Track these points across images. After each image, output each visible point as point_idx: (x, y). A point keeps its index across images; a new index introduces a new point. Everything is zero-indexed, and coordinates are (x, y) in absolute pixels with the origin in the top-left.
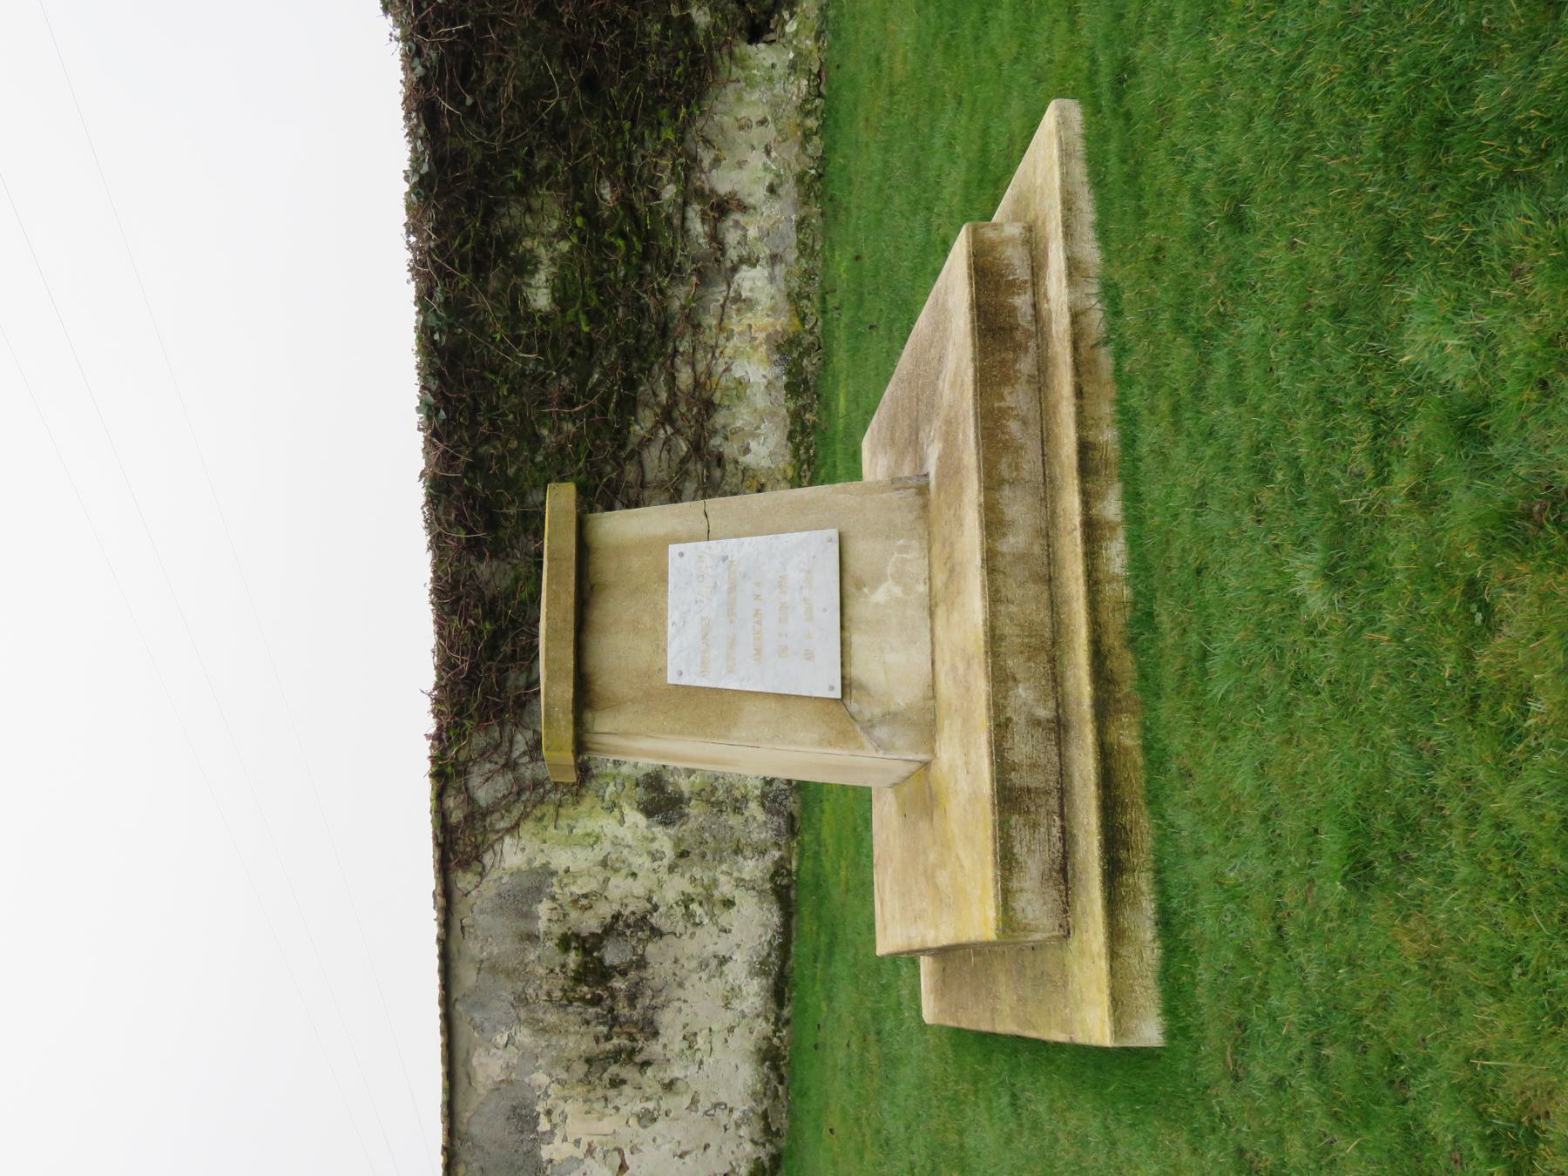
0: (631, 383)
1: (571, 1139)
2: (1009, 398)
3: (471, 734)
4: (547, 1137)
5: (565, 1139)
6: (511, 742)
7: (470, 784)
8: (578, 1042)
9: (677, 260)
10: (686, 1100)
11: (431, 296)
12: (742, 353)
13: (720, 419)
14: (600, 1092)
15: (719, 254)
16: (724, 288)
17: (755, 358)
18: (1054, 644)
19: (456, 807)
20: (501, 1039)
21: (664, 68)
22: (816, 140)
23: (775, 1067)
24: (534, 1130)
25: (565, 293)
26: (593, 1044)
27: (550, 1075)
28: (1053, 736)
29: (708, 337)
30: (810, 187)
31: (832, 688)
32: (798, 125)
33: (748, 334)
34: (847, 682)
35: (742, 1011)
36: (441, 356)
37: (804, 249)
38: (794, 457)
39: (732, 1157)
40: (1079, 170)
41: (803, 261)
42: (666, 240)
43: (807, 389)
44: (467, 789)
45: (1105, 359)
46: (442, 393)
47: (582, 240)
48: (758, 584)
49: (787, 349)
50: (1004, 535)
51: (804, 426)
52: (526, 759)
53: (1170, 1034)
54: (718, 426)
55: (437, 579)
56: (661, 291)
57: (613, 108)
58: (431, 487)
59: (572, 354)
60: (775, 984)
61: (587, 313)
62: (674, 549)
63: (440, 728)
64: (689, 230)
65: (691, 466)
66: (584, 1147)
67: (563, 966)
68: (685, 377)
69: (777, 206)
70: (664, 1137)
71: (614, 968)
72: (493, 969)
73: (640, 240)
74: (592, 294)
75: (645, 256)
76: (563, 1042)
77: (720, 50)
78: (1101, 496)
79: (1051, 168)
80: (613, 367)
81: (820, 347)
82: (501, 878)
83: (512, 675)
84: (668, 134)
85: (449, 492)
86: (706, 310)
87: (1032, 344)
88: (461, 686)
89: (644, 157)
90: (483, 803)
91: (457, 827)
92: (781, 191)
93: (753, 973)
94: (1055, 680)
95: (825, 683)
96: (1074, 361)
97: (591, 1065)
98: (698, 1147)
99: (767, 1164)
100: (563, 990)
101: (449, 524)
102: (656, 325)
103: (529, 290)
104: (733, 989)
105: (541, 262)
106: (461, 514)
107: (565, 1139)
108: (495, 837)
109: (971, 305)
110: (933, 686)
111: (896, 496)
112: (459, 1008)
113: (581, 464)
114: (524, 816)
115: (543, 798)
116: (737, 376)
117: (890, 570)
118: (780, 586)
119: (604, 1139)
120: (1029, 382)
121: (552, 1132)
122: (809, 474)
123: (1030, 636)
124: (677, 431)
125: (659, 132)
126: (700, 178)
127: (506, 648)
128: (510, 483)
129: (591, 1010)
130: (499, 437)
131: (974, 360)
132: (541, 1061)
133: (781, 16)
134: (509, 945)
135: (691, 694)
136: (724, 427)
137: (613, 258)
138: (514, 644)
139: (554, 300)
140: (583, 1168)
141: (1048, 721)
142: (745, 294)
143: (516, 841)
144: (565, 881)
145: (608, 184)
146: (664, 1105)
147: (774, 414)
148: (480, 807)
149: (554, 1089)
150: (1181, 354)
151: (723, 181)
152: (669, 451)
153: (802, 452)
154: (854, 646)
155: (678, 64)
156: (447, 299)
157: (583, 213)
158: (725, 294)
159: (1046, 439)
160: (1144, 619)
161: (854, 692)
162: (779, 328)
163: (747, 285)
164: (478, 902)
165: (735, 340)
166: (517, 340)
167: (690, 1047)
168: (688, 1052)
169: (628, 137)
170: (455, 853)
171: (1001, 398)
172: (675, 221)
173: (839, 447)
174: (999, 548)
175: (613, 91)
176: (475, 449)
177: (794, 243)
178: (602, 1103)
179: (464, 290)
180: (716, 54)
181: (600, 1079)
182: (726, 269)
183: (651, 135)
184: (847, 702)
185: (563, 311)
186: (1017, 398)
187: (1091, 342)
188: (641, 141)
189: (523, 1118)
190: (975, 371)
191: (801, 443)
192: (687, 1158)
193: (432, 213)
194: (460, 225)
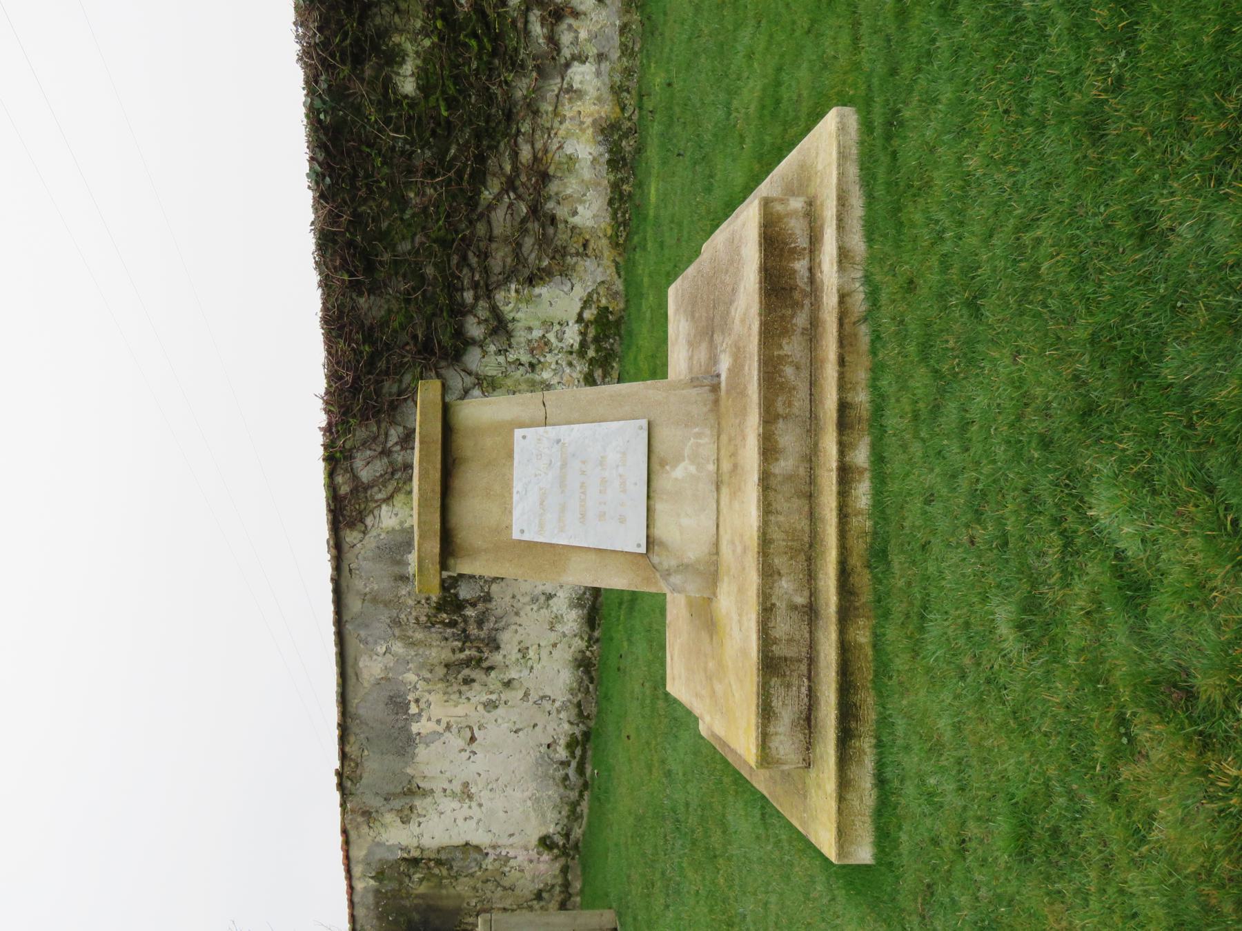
0: (481, 159)
1: (434, 719)
2: (786, 347)
3: (355, 430)
4: (416, 717)
5: (429, 719)
6: (387, 435)
7: (355, 466)
8: (439, 651)
9: (520, 57)
10: (521, 694)
11: (316, 82)
12: (573, 134)
13: (553, 187)
14: (455, 688)
16: (559, 80)
17: (583, 139)
18: (811, 546)
19: (344, 483)
20: (381, 649)
24: (406, 713)
25: (428, 81)
26: (451, 654)
29: (544, 121)
31: (639, 546)
33: (577, 119)
34: (651, 540)
35: (563, 632)
36: (326, 134)
37: (625, 50)
38: (613, 219)
39: (553, 733)
40: (853, 171)
41: (624, 59)
42: (511, 40)
43: (625, 165)
44: (352, 469)
45: (864, 330)
46: (328, 163)
47: (442, 39)
48: (584, 462)
49: (609, 131)
50: (777, 460)
51: (621, 194)
52: (398, 448)
54: (552, 194)
55: (325, 309)
56: (506, 82)
58: (319, 238)
60: (589, 614)
61: (446, 100)
62: (518, 433)
63: (330, 424)
64: (530, 32)
66: (444, 725)
68: (526, 153)
70: (503, 718)
71: (467, 601)
72: (375, 600)
73: (490, 40)
74: (450, 83)
75: (494, 53)
78: (853, 446)
79: (829, 164)
80: (467, 145)
82: (379, 535)
83: (387, 384)
85: (335, 242)
86: (543, 98)
87: (807, 302)
88: (347, 394)
90: (365, 480)
91: (345, 497)
93: (572, 606)
94: (810, 576)
95: (634, 541)
97: (449, 669)
98: (529, 726)
99: (580, 738)
100: (427, 615)
101: (335, 268)
102: (503, 111)
103: (397, 78)
104: (556, 617)
105: (408, 55)
106: (343, 259)
107: (429, 719)
108: (374, 505)
109: (760, 268)
110: (717, 544)
111: (694, 391)
112: (349, 627)
113: (441, 223)
114: (397, 490)
116: (568, 153)
117: (687, 452)
119: (459, 719)
120: (802, 334)
121: (419, 714)
122: (624, 234)
123: (793, 540)
124: (519, 197)
127: (382, 364)
128: (383, 236)
129: (449, 630)
130: (374, 199)
131: (760, 315)
132: (411, 665)
134: (386, 584)
135: (531, 546)
136: (557, 194)
137: (467, 55)
138: (388, 362)
139: (419, 87)
140: (443, 739)
141: (803, 606)
142: (575, 87)
143: (390, 508)
146: (504, 697)
148: (363, 483)
150: (920, 380)
152: (512, 214)
153: (619, 215)
154: (657, 512)
156: (330, 86)
157: (443, 17)
159: (814, 383)
160: (879, 555)
161: (656, 548)
162: (603, 114)
163: (577, 78)
164: (362, 552)
165: (567, 124)
166: (388, 121)
168: (522, 661)
170: (343, 516)
171: (780, 347)
172: (519, 24)
176: (355, 210)
177: (617, 44)
178: (458, 695)
179: (344, 79)
181: (456, 678)
182: (561, 65)
184: (650, 555)
185: (426, 97)
186: (793, 347)
187: (853, 319)
189: (398, 704)
190: (761, 324)
191: (619, 208)
192: (520, 733)
193: (316, 14)
194: (340, 23)
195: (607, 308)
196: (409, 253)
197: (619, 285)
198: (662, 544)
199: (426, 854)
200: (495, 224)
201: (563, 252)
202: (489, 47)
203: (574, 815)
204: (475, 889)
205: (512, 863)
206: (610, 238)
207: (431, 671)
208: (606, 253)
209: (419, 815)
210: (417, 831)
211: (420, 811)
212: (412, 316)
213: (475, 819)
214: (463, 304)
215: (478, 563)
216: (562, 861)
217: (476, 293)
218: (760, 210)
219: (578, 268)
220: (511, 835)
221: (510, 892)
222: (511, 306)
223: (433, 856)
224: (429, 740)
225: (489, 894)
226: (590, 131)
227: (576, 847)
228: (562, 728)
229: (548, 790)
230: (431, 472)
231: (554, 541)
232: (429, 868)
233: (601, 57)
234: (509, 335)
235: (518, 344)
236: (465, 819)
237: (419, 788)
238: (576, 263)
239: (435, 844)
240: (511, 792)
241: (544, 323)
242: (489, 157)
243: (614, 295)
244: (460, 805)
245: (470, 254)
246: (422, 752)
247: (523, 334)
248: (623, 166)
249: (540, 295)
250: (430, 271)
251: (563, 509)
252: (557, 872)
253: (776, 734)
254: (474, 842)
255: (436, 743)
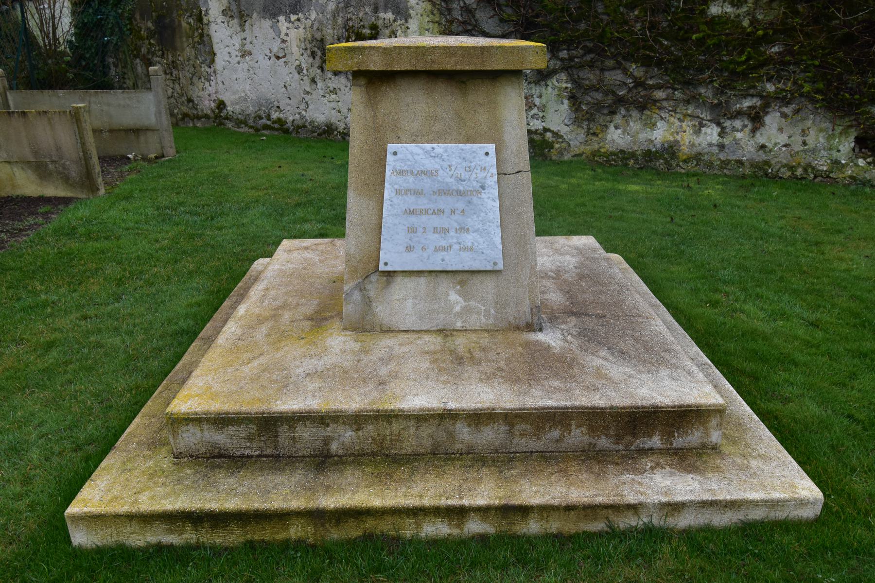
0: (659, 64)
1: (288, 31)
5: (288, 28)
10: (308, 89)
12: (670, 127)
13: (635, 114)
14: (309, 46)
15: (728, 116)
16: (709, 118)
17: (667, 134)
21: (849, 85)
22: (789, 174)
23: (324, 132)
24: (291, 12)
25: (717, 24)
27: (315, 20)
28: (317, 452)
29: (681, 108)
30: (760, 169)
32: (799, 164)
34: (392, 274)
37: (725, 163)
38: (611, 153)
40: (756, 515)
41: (719, 163)
42: (742, 85)
43: (647, 161)
45: (598, 526)
47: (748, 35)
48: (463, 212)
49: (670, 150)
50: (469, 426)
51: (627, 159)
53: (79, 553)
56: (712, 82)
57: (829, 54)
59: (680, 29)
61: (704, 38)
62: (491, 148)
64: (745, 98)
65: (610, 97)
66: (285, 38)
67: (364, 26)
68: (660, 94)
69: (752, 150)
75: (733, 73)
76: (329, 27)
77: (855, 120)
80: (671, 53)
81: (668, 173)
84: (807, 88)
86: (697, 107)
89: (794, 72)
92: (761, 152)
96: (596, 505)
99: (285, 127)
100: (353, 26)
105: (738, 8)
109: (657, 407)
111: (527, 309)
113: (616, 34)
115: (443, 14)
116: (658, 124)
117: (473, 304)
118: (461, 228)
120: (590, 444)
121: (290, 22)
122: (601, 161)
124: (630, 90)
125: (809, 82)
126: (776, 105)
131: (611, 408)
132: (321, 15)
133: (869, 156)
136: (630, 116)
139: (714, 17)
140: (276, 38)
142: (703, 129)
144: (403, 27)
145: (781, 49)
147: (635, 143)
149: (309, 23)
151: (772, 120)
152: (619, 85)
155: (851, 94)
157: (765, 35)
158: (705, 118)
161: (385, 278)
162: (682, 147)
163: (709, 131)
165: (678, 123)
167: (331, 91)
169: (809, 62)
171: (579, 426)
173: (609, 185)
174: (459, 422)
175: (841, 54)
178: (304, 47)
180: (853, 117)
183: (808, 77)
185: (707, 23)
186: (578, 436)
188: (804, 71)
190: (602, 408)
192: (284, 89)
195: (552, 148)
196: (596, 11)
197: (567, 157)
198: (388, 283)
199: (205, 27)
200: (612, 73)
201: (591, 119)
202: (739, 69)
203: (239, 123)
204: (189, 60)
205: (207, 84)
206: (598, 151)
207: (318, 29)
208: (588, 148)
209: (228, 22)
210: (219, 21)
211: (231, 22)
212: (551, 14)
213: (230, 60)
214: (559, 50)
215: (362, 108)
216: (212, 115)
217: (566, 59)
218: (714, 405)
219: (579, 129)
220: (223, 82)
221: (190, 82)
222: (556, 84)
223: (205, 32)
224: (275, 27)
225: (187, 68)
226: (672, 139)
227: (221, 124)
228: (290, 115)
229: (252, 106)
230: (452, 60)
231: (386, 184)
232: (197, 29)
233: (722, 147)
234: (537, 83)
235: (531, 89)
236: (229, 53)
237: (245, 22)
238: (583, 128)
239: (212, 33)
240: (249, 83)
241: (544, 106)
242: (659, 69)
243: (561, 152)
244: (237, 49)
245: (592, 56)
246: (267, 23)
247: (537, 92)
248: (646, 160)
249: (562, 103)
250: (583, 26)
251: (418, 193)
252: (205, 112)
253: (202, 430)
254: (216, 59)
255: (273, 33)
